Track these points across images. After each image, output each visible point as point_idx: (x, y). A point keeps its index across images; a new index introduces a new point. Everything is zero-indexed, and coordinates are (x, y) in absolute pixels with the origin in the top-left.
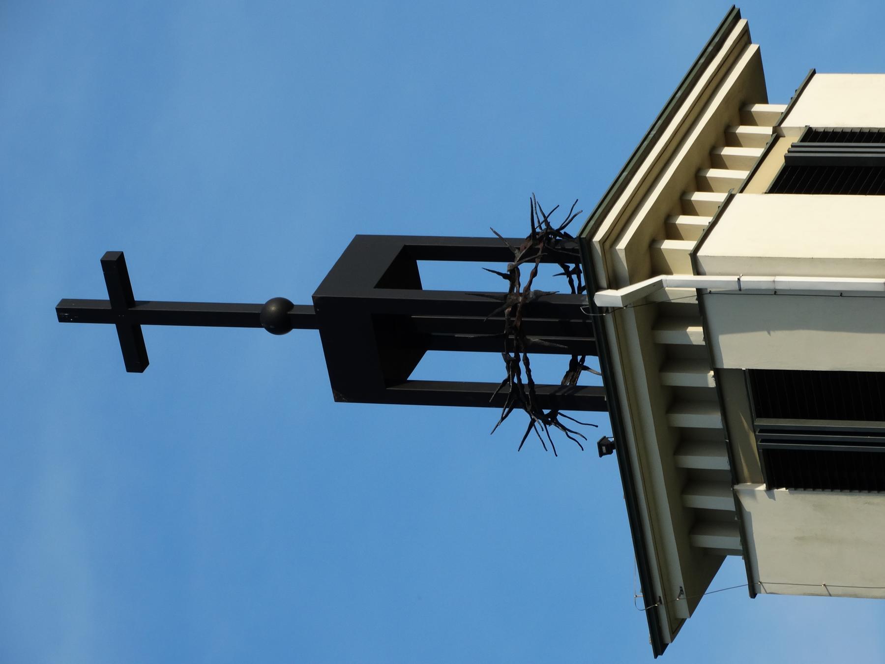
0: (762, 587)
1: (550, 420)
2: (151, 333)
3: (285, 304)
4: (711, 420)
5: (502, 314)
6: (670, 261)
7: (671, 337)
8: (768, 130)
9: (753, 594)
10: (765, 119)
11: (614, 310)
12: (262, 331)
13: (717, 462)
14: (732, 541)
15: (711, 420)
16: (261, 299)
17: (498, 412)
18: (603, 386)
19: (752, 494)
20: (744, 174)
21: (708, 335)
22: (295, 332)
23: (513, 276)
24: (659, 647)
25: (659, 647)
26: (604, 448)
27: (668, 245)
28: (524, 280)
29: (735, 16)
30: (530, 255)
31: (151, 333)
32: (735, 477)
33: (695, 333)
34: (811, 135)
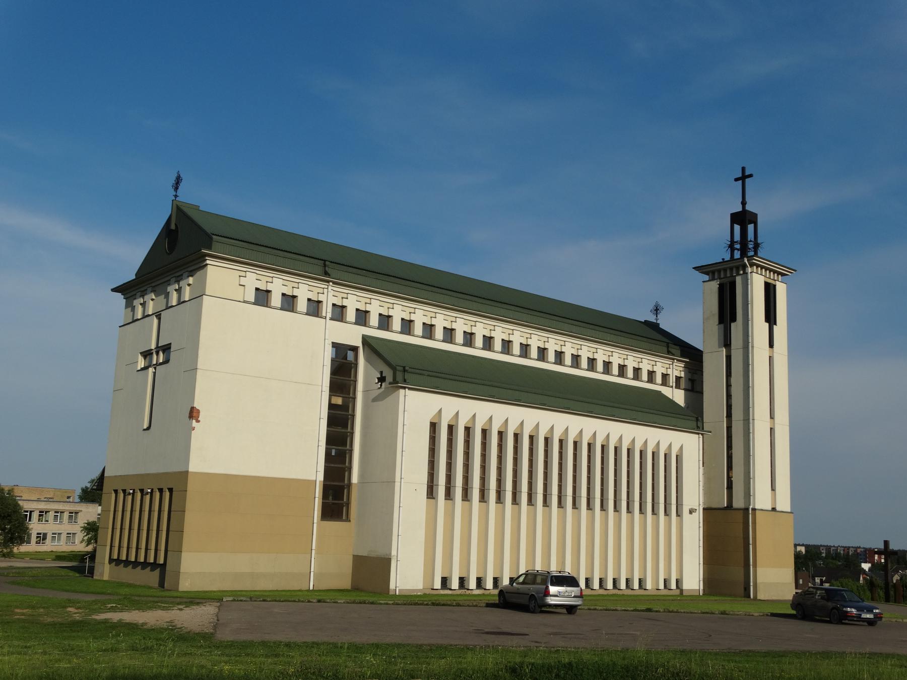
0: (694, 415)
1: (729, 247)
2: (740, 182)
3: (746, 204)
4: (728, 275)
5: (454, 667)
6: (752, 268)
7: (741, 268)
8: (776, 279)
9: (703, 282)
10: (778, 278)
11: (744, 261)
12: (741, 200)
13: (722, 276)
14: (711, 279)
15: (728, 275)
16: (747, 200)
17: (730, 240)
18: (504, 585)
19: (717, 282)
20: (768, 276)
21: (741, 274)
22: (741, 206)
23: (751, 241)
24: (693, 268)
25: (693, 268)
26: (723, 259)
27: (755, 267)
28: (750, 243)
29: (795, 271)
30: (755, 244)
31: (740, 182)
32: (720, 278)
33: (741, 272)
34: (775, 286)
